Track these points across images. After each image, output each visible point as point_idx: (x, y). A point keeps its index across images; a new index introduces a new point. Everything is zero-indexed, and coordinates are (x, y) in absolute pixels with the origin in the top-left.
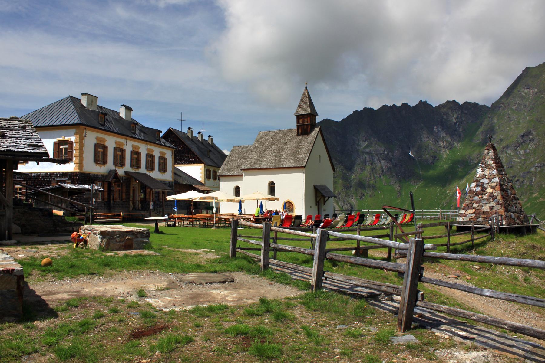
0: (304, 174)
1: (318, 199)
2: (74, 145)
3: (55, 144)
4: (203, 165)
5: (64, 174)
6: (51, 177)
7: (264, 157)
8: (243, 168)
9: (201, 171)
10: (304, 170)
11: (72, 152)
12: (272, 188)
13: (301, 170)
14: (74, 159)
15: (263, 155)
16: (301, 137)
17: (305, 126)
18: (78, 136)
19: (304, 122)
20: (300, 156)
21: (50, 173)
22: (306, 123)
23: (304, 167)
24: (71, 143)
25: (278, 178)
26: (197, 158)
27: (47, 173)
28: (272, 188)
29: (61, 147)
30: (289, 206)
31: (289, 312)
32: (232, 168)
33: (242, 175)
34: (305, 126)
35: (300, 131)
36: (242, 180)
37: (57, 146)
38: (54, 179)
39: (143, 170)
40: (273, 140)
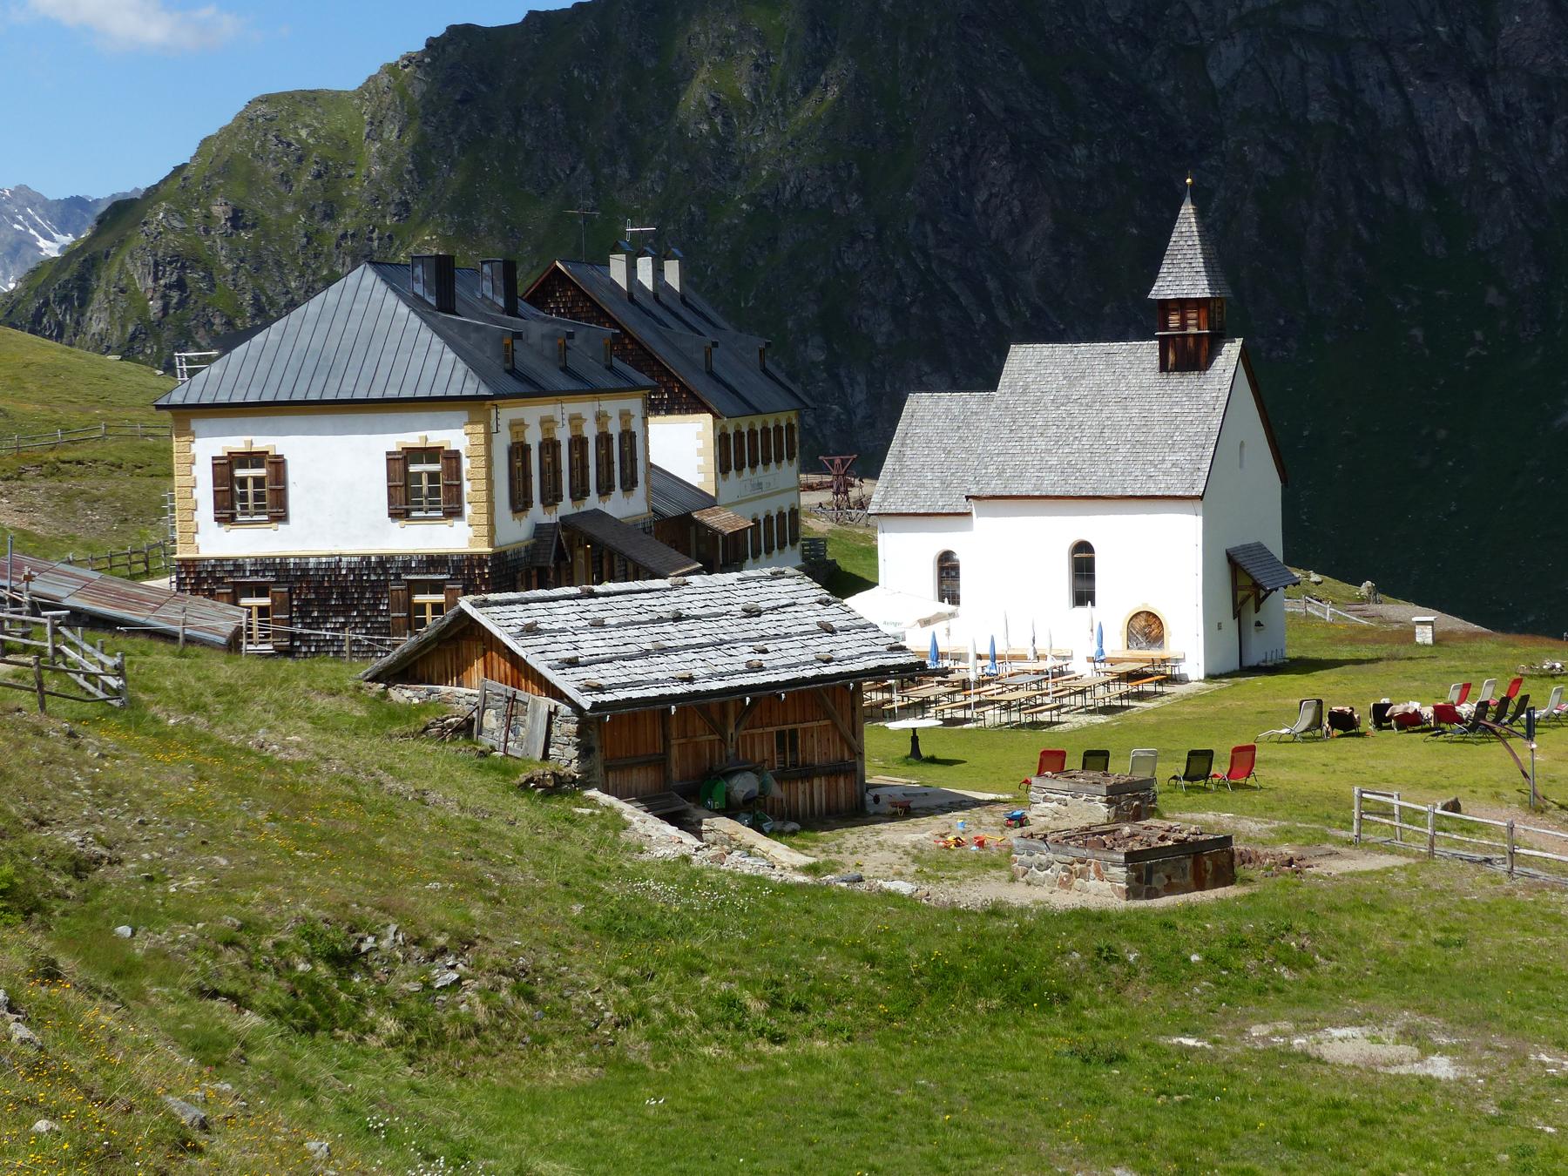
0: (1200, 519)
1: (1241, 594)
2: (466, 464)
3: (391, 458)
4: (708, 417)
5: (434, 562)
6: (386, 571)
7: (1049, 451)
8: (974, 491)
9: (700, 444)
10: (1199, 505)
11: (459, 487)
12: (1083, 562)
13: (1189, 503)
14: (468, 509)
15: (1042, 443)
16: (1175, 377)
17: (1191, 341)
18: (480, 428)
19: (1184, 326)
20: (1179, 456)
21: (380, 556)
22: (1194, 331)
23: (1201, 498)
24: (454, 457)
25: (1106, 531)
26: (683, 387)
27: (366, 558)
28: (1083, 562)
29: (413, 468)
30: (1147, 627)
31: (202, 1140)
32: (922, 486)
33: (969, 514)
34: (1191, 341)
35: (1171, 357)
36: (970, 528)
37: (399, 466)
38: (398, 576)
39: (592, 502)
40: (1071, 385)
